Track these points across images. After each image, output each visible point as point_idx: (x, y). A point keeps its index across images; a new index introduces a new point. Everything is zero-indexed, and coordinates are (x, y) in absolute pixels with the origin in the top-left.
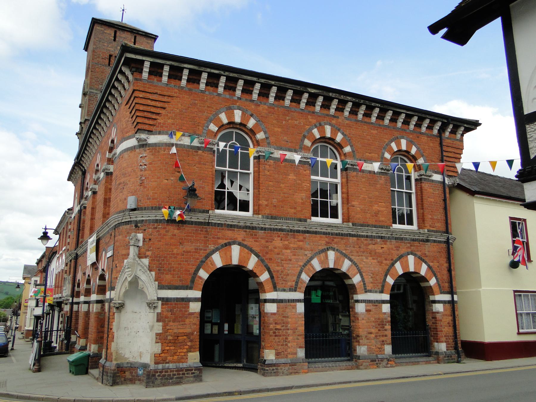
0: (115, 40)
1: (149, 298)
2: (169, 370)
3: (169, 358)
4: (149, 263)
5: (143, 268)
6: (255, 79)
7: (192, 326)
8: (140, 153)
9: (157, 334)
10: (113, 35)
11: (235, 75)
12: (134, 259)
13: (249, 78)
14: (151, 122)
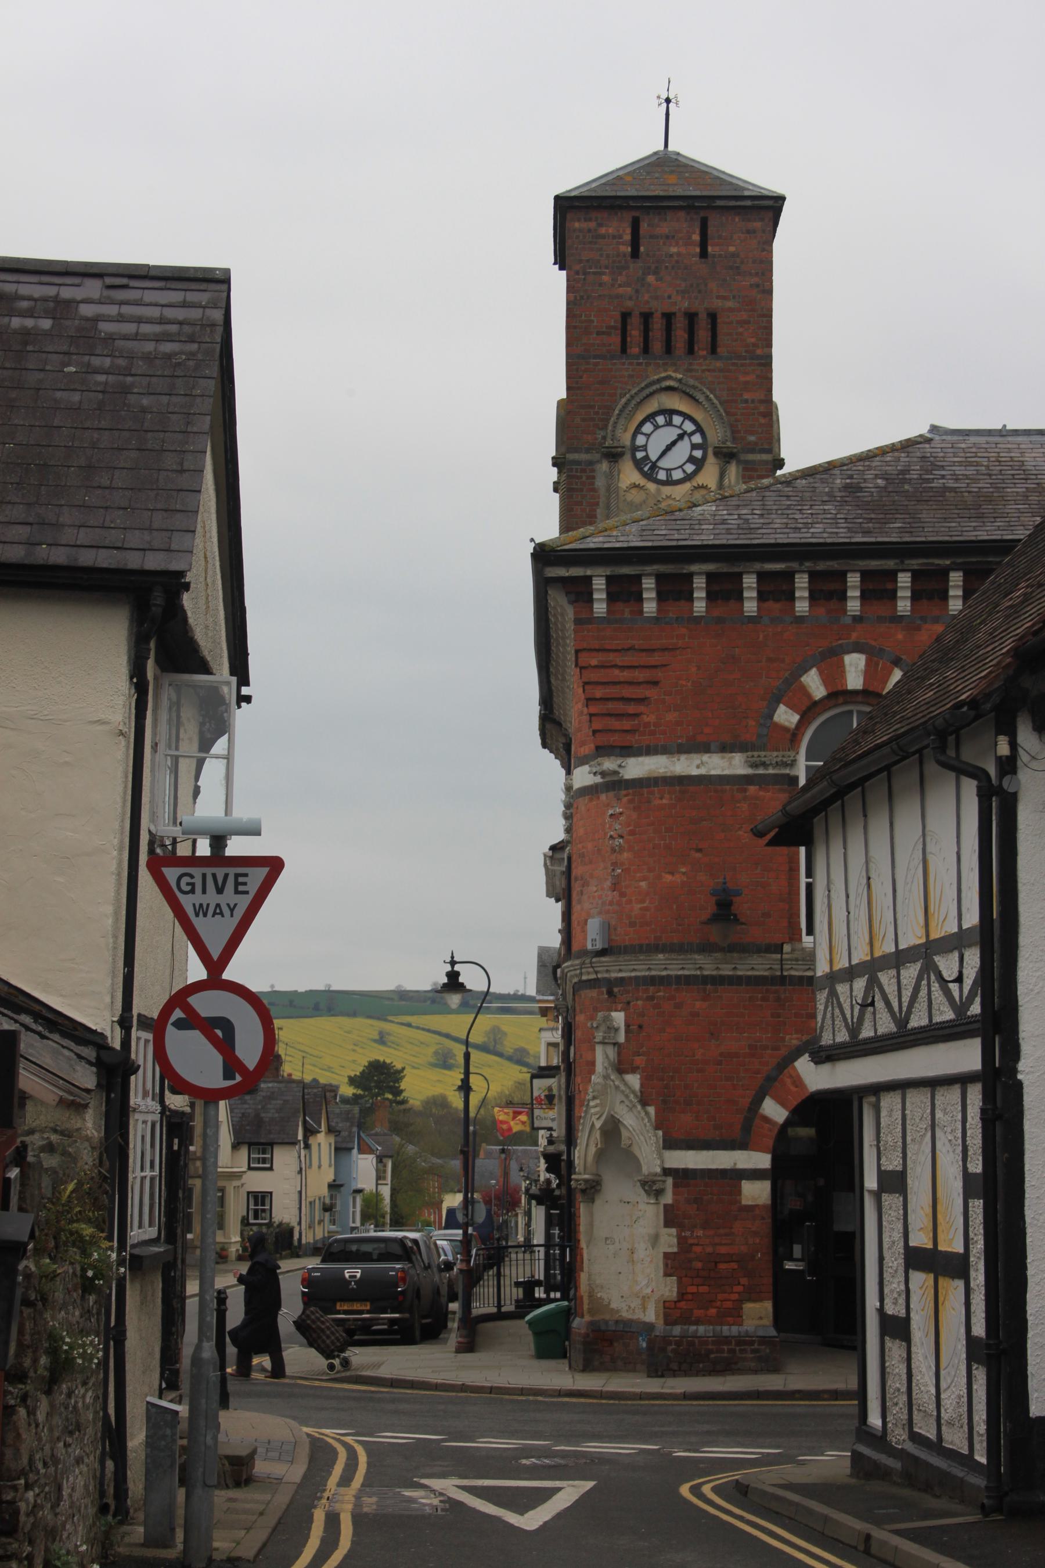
0: (635, 254)
1: (645, 1170)
2: (696, 1341)
3: (698, 1313)
4: (642, 1085)
5: (627, 1096)
6: (890, 564)
7: (751, 1240)
8: (608, 805)
9: (666, 1255)
10: (628, 237)
11: (834, 565)
12: (606, 1077)
13: (874, 564)
14: (627, 724)
